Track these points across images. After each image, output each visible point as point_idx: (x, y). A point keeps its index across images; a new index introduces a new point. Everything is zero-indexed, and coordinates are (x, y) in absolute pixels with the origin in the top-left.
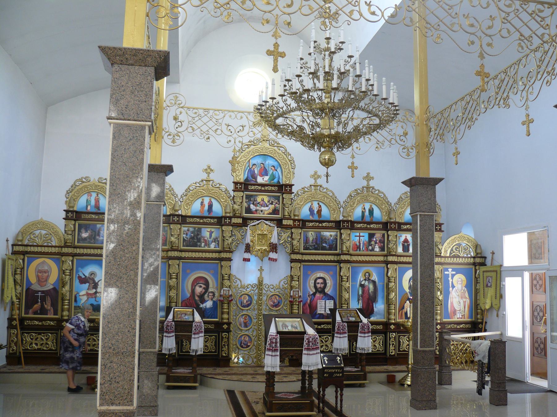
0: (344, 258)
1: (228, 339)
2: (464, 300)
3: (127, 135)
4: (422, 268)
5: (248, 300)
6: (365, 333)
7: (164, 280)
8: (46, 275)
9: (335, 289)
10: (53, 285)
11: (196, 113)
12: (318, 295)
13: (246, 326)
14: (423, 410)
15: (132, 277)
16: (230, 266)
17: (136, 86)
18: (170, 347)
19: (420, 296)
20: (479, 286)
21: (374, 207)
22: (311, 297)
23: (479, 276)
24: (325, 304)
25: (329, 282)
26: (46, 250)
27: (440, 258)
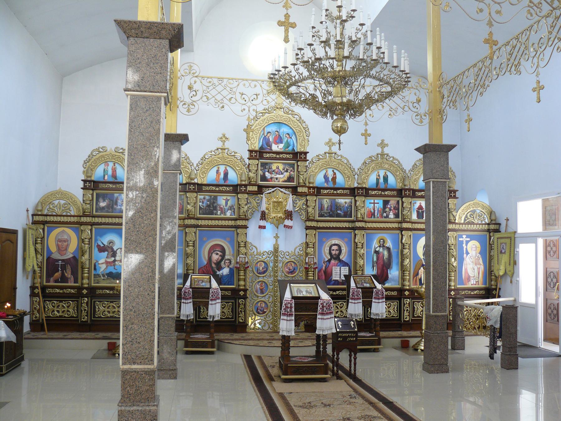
0: (358, 224)
1: (245, 305)
2: (479, 266)
3: (144, 107)
4: (435, 234)
5: (264, 266)
6: (379, 299)
7: (181, 247)
8: (66, 244)
9: (349, 255)
10: (73, 253)
11: (210, 82)
12: (333, 261)
13: (262, 292)
14: (435, 373)
15: (151, 243)
16: (246, 233)
17: (151, 58)
18: (188, 313)
19: (433, 262)
20: (494, 252)
21: (389, 174)
22: (326, 264)
23: (494, 242)
24: (340, 270)
25: (344, 249)
26: (65, 219)
27: (454, 225)
